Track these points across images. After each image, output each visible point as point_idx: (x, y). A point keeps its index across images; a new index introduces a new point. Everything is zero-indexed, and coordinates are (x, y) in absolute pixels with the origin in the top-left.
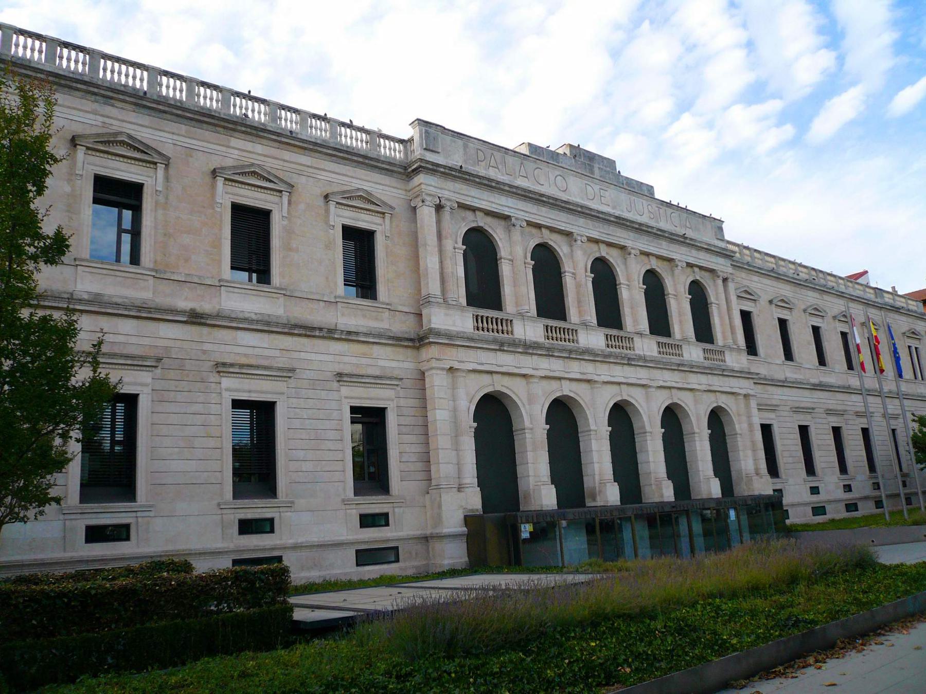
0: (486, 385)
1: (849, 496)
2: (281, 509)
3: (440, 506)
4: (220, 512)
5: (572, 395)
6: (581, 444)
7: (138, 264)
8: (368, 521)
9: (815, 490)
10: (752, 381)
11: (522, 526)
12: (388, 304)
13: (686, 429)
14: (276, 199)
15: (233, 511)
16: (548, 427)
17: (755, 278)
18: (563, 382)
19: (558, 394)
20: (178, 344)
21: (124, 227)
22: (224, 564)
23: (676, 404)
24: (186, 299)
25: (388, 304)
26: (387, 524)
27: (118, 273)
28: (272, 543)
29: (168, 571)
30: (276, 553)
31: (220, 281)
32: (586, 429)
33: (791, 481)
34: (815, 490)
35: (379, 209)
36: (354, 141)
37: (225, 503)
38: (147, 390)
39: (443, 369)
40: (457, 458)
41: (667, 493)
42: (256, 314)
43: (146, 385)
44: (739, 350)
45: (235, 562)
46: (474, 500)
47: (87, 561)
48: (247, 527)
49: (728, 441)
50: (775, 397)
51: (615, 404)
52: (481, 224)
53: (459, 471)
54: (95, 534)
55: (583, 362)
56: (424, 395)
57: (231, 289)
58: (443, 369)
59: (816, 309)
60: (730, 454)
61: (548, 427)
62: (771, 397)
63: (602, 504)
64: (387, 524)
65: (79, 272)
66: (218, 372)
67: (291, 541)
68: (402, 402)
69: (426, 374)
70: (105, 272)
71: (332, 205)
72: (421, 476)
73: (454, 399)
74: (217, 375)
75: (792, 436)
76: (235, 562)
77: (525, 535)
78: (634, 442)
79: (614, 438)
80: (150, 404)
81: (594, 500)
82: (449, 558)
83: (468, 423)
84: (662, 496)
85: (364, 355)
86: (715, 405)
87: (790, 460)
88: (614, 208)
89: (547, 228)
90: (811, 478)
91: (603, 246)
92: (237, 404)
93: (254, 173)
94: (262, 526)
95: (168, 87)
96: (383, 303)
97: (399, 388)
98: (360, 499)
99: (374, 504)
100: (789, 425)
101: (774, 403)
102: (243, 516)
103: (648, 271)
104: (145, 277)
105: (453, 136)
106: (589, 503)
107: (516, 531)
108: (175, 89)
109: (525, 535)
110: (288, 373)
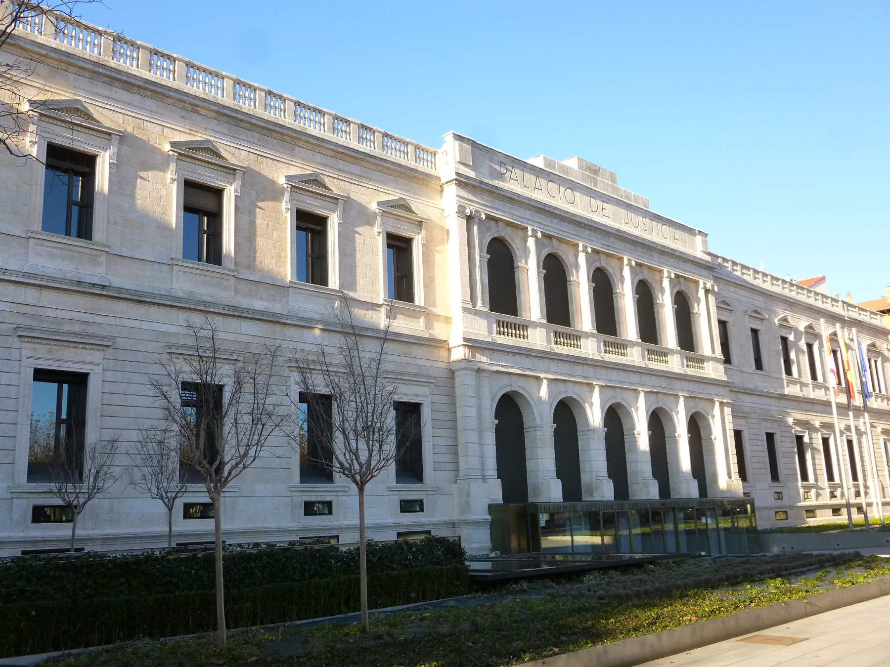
0: (501, 388)
1: (779, 503)
2: (339, 494)
3: (468, 496)
4: (290, 494)
5: (575, 396)
6: (580, 443)
7: (220, 264)
8: (408, 506)
9: (779, 495)
10: (728, 389)
11: (541, 516)
12: (104, 246)
13: (527, 422)
15: (300, 494)
16: (497, 421)
17: (732, 289)
18: (659, 395)
19: (508, 389)
20: (257, 340)
21: (74, 199)
22: (390, 537)
23: (571, 398)
24: (261, 298)
25: (104, 246)
26: (422, 510)
27: (206, 273)
28: (331, 524)
29: (715, 518)
30: (334, 533)
31: (27, 232)
32: (584, 429)
33: (758, 486)
34: (779, 495)
37: (293, 487)
38: (98, 369)
39: (472, 370)
40: (482, 449)
41: (652, 492)
42: (318, 314)
43: (98, 364)
44: (716, 360)
45: (399, 535)
46: (494, 491)
47: (186, 535)
48: (309, 508)
49: (703, 445)
50: (746, 404)
51: (504, 395)
52: (502, 234)
53: (483, 464)
55: (585, 367)
56: (454, 392)
57: (298, 291)
58: (472, 370)
59: (756, 312)
60: (705, 457)
61: (497, 421)
62: (742, 404)
63: (598, 499)
64: (422, 510)
65: (175, 271)
66: (19, 336)
67: (346, 522)
68: (437, 399)
69: (456, 374)
70: (195, 271)
72: (450, 466)
73: (479, 397)
74: (16, 339)
75: (760, 443)
76: (399, 535)
77: (542, 524)
78: (701, 447)
79: (558, 436)
81: (592, 495)
82: (477, 542)
83: (490, 421)
84: (649, 494)
85: (405, 355)
86: (694, 410)
87: (758, 466)
88: (614, 220)
89: (557, 238)
90: (775, 484)
91: (603, 257)
92: (41, 375)
94: (66, 513)
97: (432, 386)
98: (402, 486)
99: (412, 491)
100: (757, 432)
101: (746, 410)
102: (308, 499)
103: (640, 281)
104: (228, 277)
105: (481, 149)
106: (585, 498)
107: (535, 518)
109: (542, 524)
110: (101, 343)
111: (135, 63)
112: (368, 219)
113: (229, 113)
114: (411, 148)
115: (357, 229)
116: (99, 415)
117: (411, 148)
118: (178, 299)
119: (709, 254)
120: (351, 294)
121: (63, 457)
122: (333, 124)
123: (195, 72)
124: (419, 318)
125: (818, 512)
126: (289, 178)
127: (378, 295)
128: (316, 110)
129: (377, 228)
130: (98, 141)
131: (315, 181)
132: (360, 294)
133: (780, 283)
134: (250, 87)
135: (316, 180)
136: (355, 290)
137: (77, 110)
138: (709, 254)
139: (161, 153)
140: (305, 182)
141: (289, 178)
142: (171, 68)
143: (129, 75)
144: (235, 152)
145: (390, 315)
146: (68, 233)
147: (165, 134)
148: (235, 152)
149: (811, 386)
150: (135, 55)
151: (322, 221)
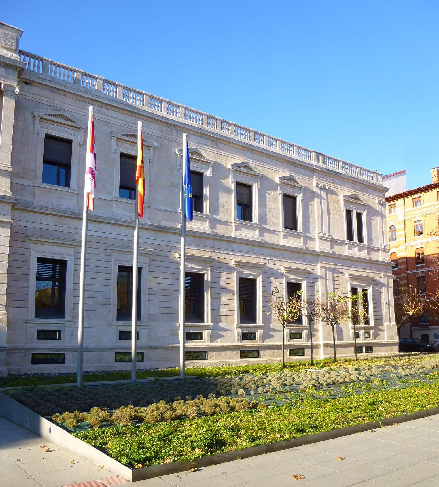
14: (77, 133)
35: (74, 124)
36: (62, 76)
47: (121, 349)
54: (43, 335)
71: (37, 120)
80: (73, 265)
93: (61, 116)
95: (56, 73)
96: (72, 189)
98: (39, 320)
108: (60, 74)
111: (201, 122)
112: (274, 187)
113: (161, 119)
114: (266, 138)
115: (372, 218)
116: (72, 283)
117: (340, 163)
118: (63, 212)
119: (21, 52)
120: (308, 234)
121: (52, 304)
122: (255, 136)
123: (128, 93)
124: (206, 221)
125: (374, 349)
126: (280, 178)
127: (231, 217)
128: (306, 150)
129: (278, 192)
130: (203, 166)
131: (292, 179)
132: (221, 217)
133: (232, 127)
134: (199, 113)
135: (246, 166)
136: (309, 233)
137: (196, 152)
138: (21, 52)
139: (274, 182)
140: (351, 198)
141: (280, 178)
142: (142, 99)
143: (302, 162)
144: (301, 180)
145: (238, 229)
146: (58, 184)
147: (277, 174)
148: (301, 180)
149: (282, 234)
150: (177, 111)
151: (294, 198)
